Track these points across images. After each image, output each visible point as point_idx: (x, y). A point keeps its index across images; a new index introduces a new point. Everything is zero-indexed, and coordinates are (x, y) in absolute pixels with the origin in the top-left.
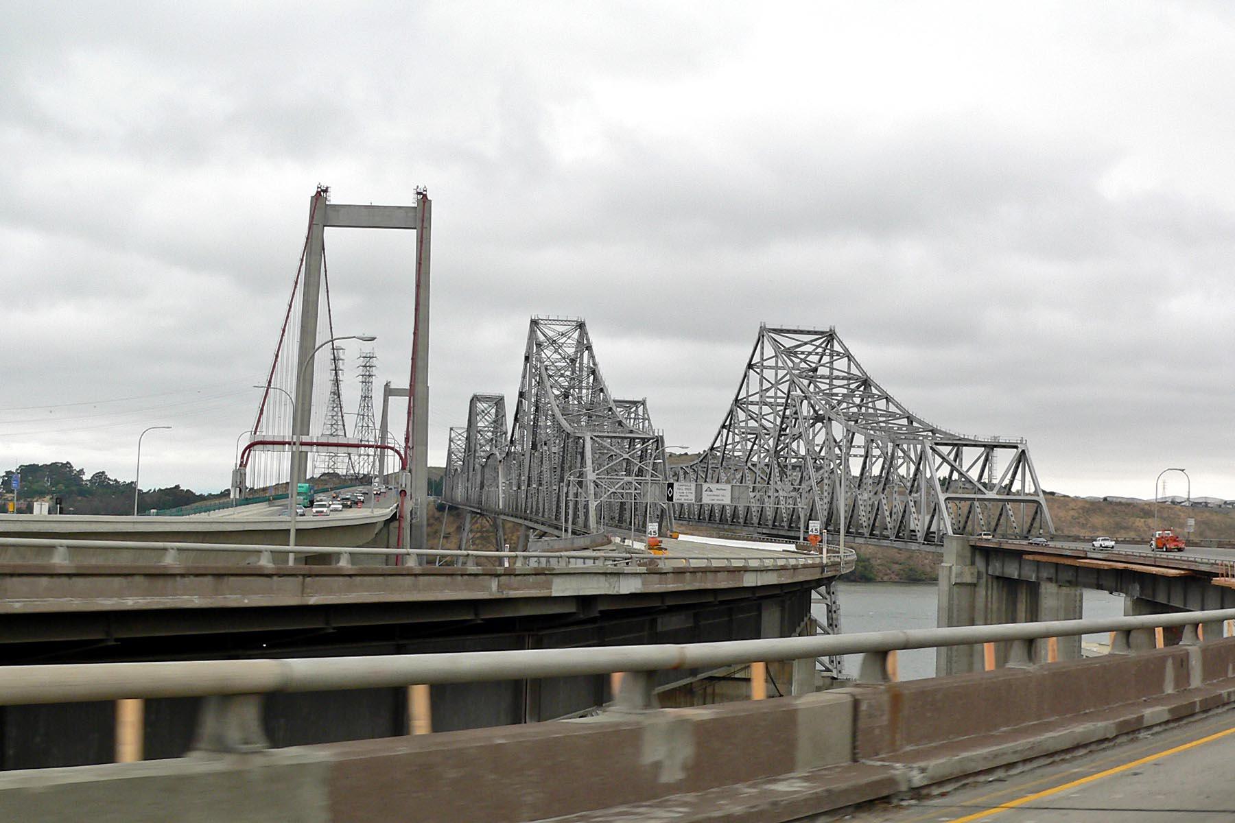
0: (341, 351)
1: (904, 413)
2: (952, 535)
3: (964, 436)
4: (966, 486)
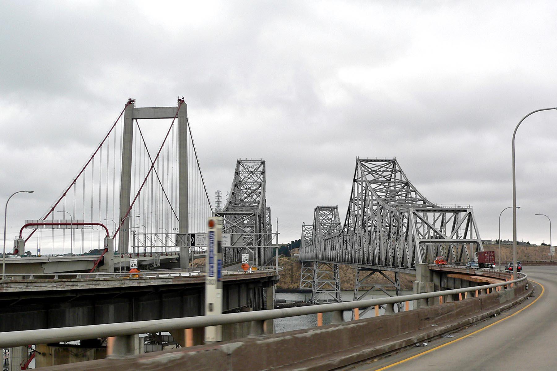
0: (220, 193)
1: (422, 198)
2: (422, 263)
3: (444, 207)
4: (509, 243)
